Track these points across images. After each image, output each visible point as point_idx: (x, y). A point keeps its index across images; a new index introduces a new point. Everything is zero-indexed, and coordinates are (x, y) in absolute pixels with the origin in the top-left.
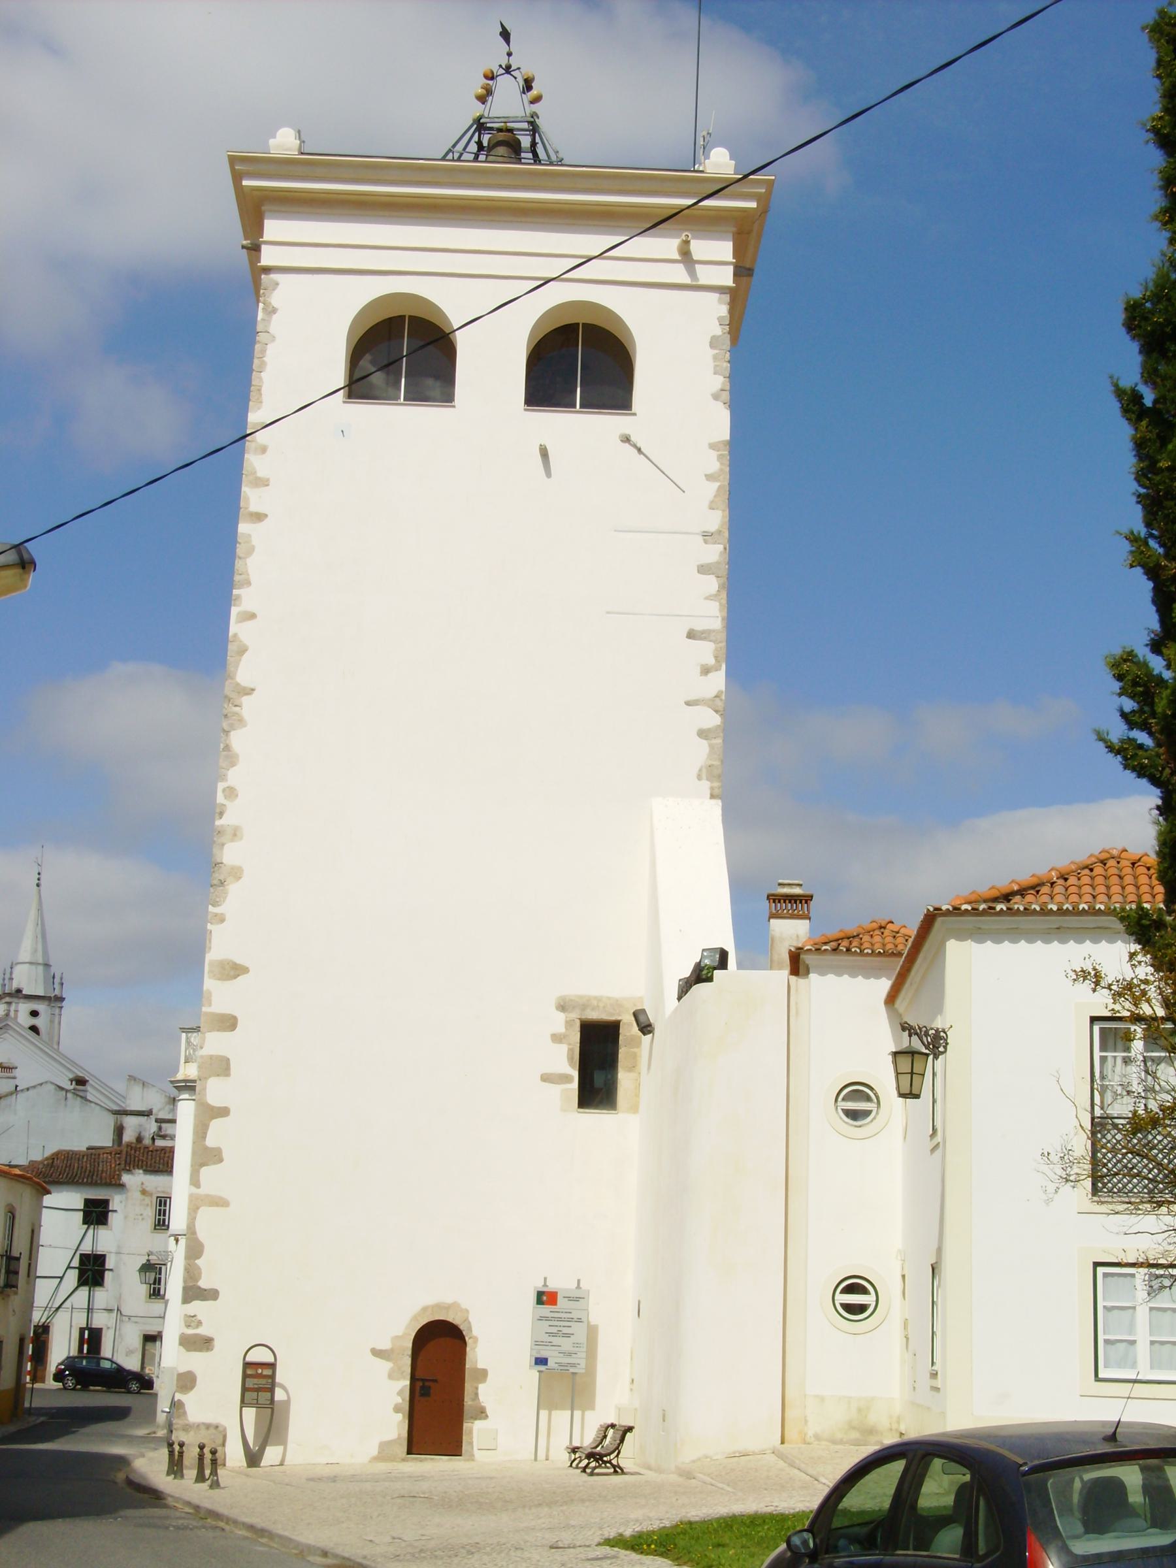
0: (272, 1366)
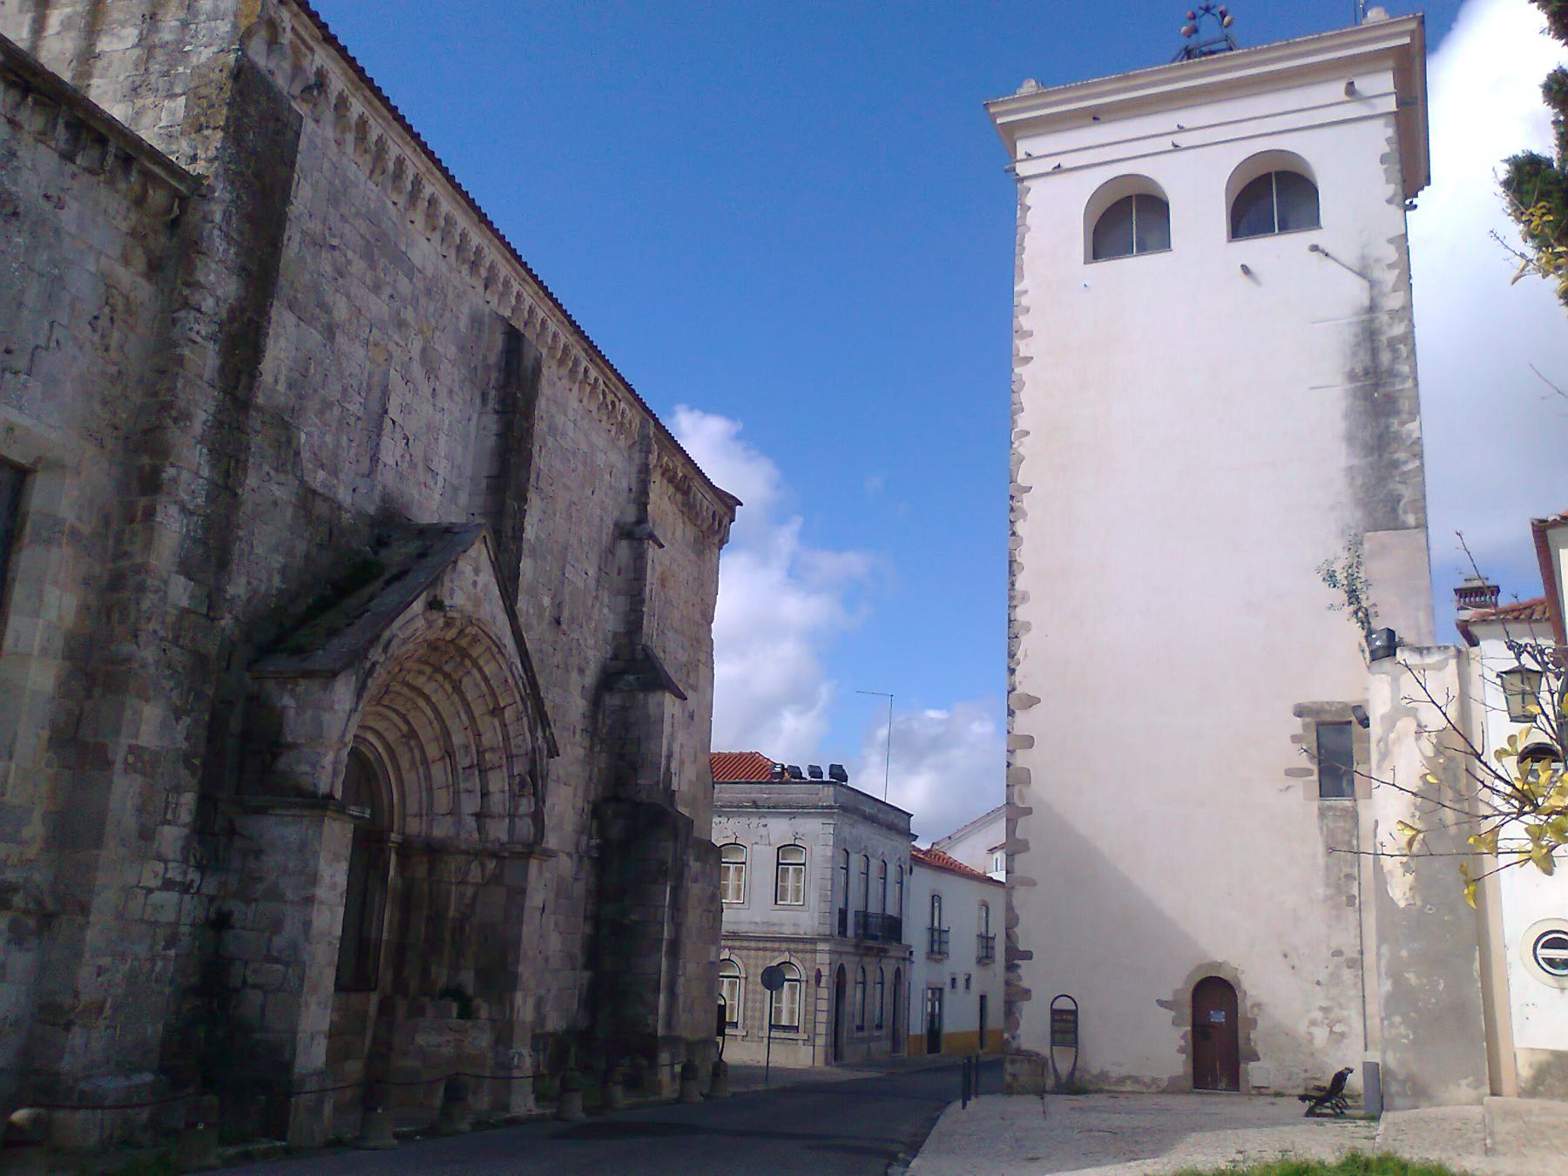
0: (1075, 1013)
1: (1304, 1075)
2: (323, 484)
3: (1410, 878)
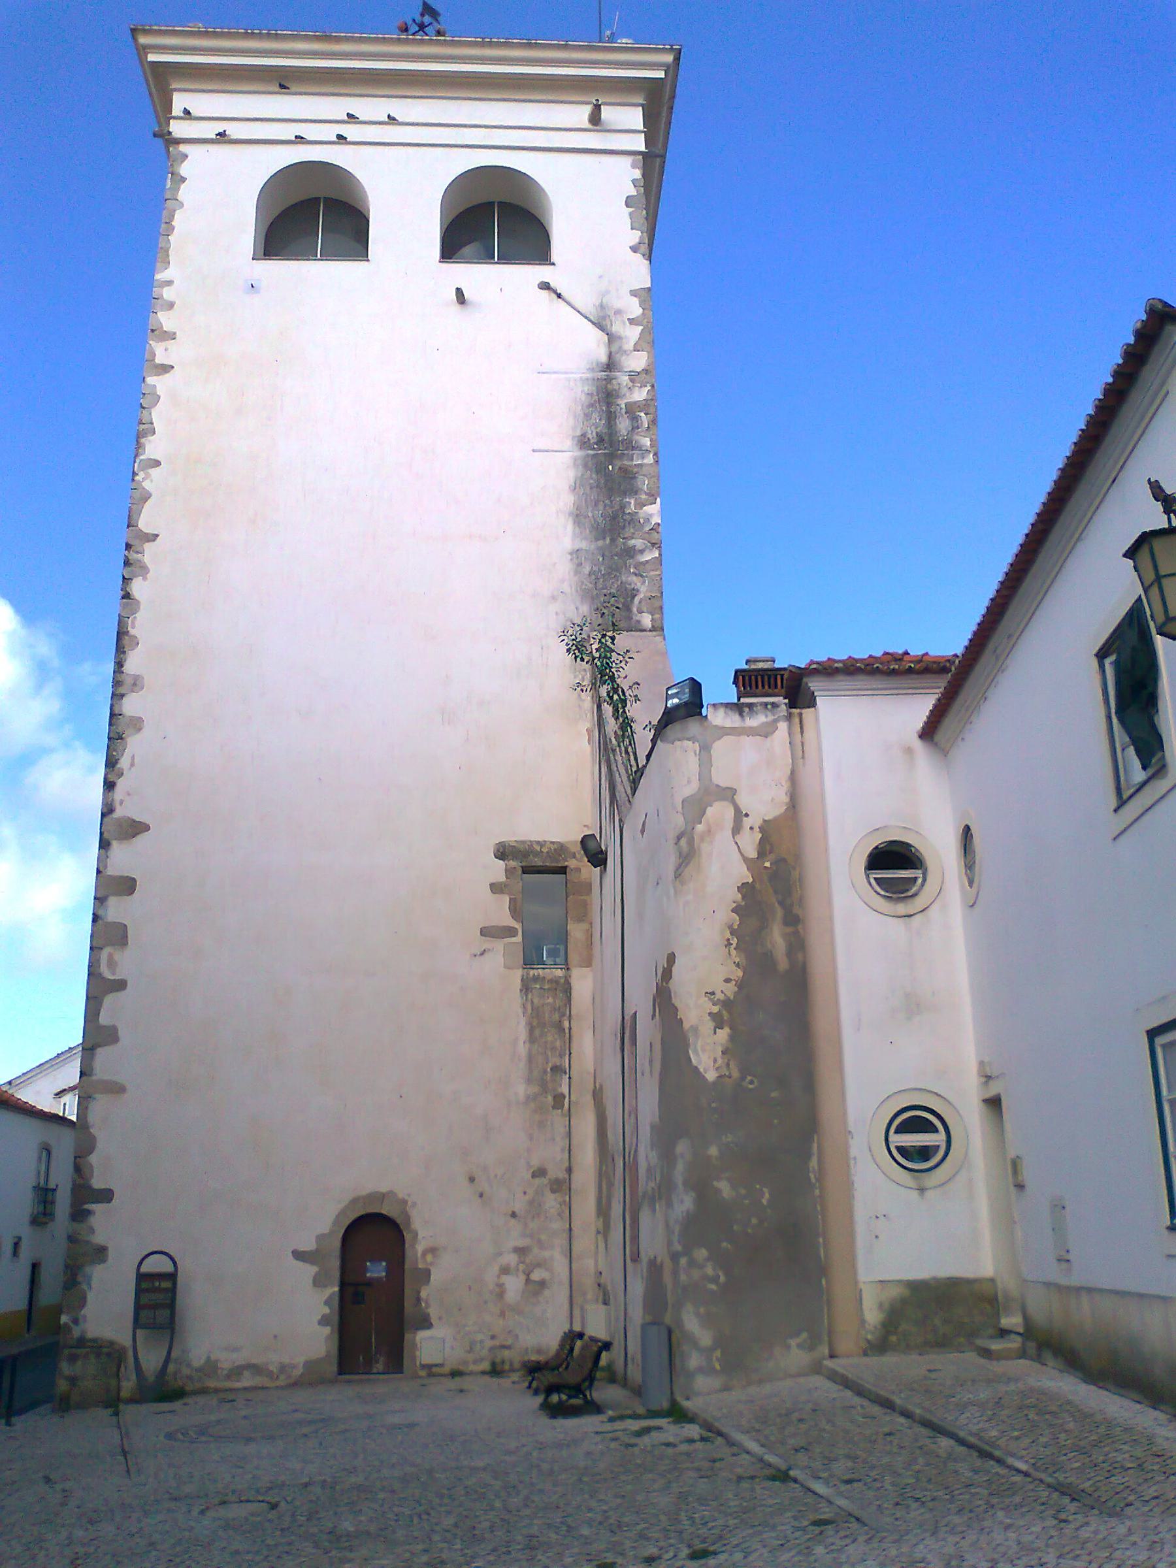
0: (172, 1277)
1: (489, 1343)
2: (66, 1324)
3: (723, 1034)
